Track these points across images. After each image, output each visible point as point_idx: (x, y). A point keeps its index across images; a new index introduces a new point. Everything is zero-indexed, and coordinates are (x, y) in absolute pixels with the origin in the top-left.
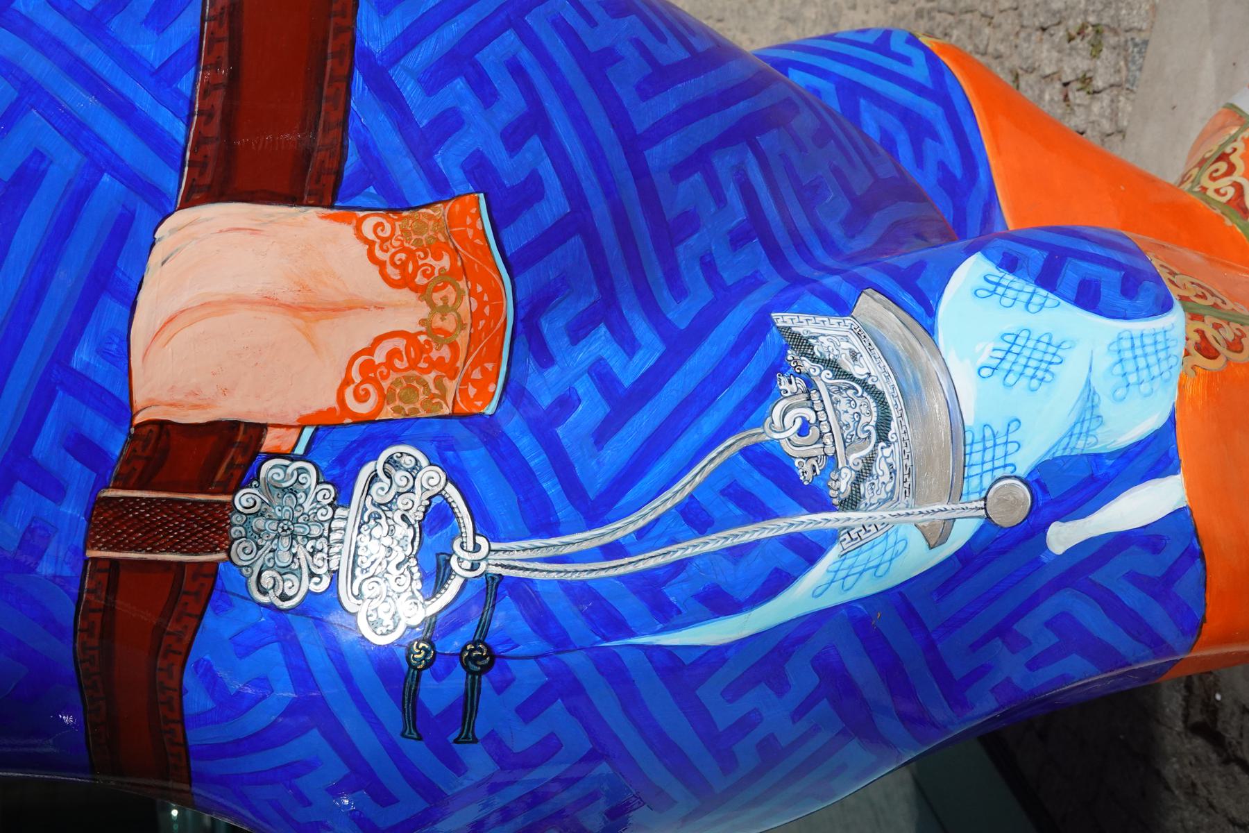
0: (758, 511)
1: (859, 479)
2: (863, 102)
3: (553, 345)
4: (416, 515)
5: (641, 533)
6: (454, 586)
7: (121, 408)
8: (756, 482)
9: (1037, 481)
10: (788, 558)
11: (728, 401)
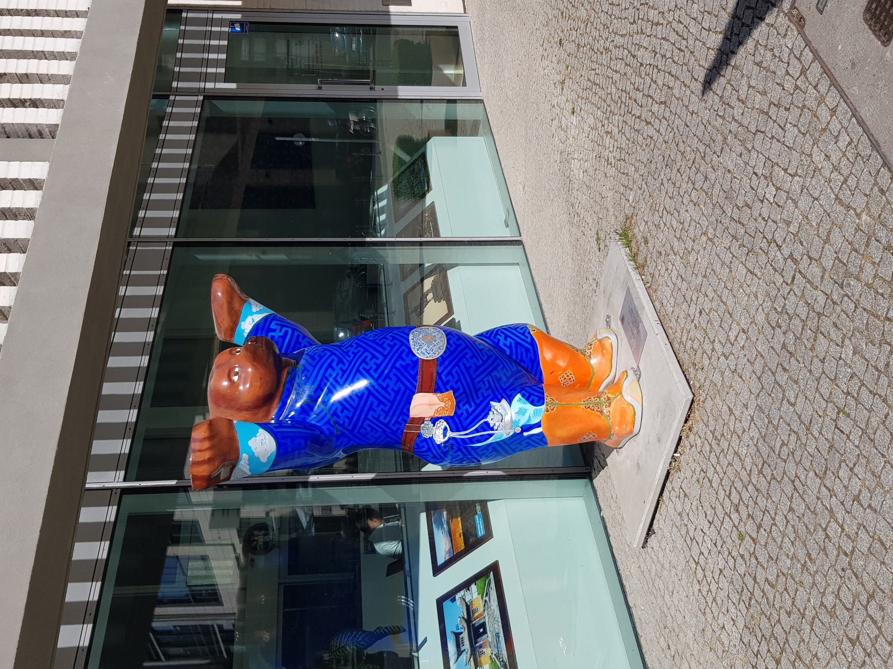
0: (485, 430)
8: (486, 427)
9: (522, 428)
10: (488, 436)
11: (483, 415)
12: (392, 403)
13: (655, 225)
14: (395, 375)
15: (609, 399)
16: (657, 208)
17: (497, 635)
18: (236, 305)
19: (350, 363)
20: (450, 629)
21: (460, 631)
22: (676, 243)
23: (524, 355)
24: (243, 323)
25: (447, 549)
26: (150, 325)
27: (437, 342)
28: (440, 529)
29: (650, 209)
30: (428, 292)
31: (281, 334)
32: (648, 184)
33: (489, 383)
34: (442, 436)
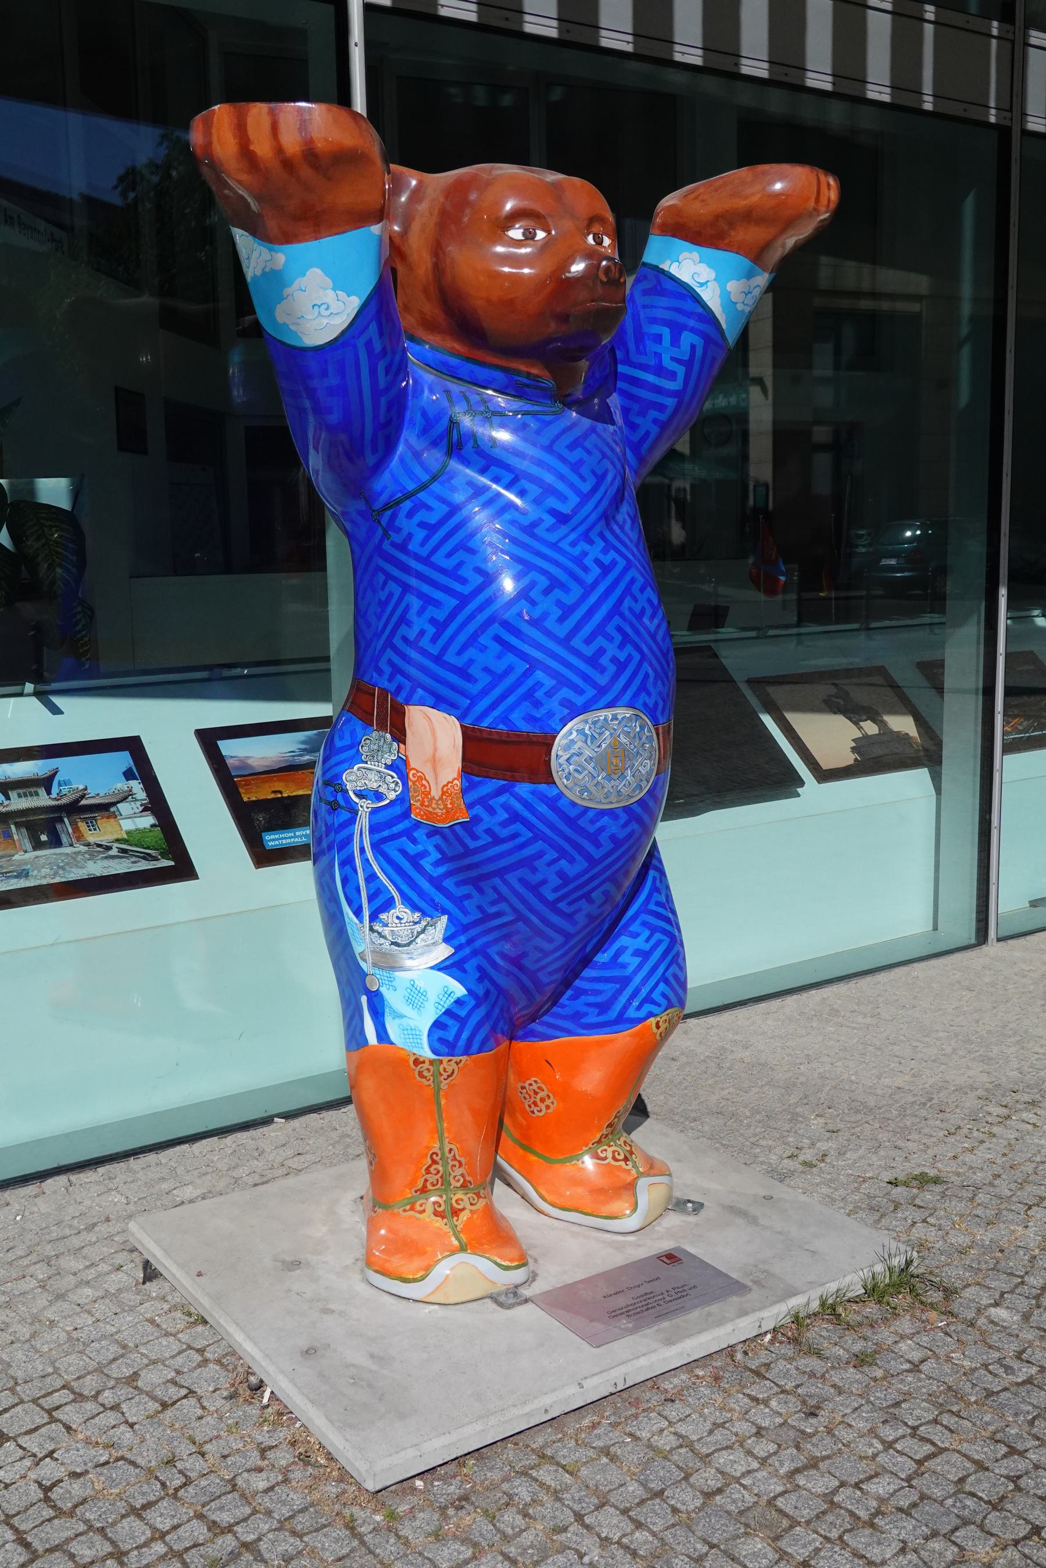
0: (371, 899)
1: (379, 933)
2: (618, 986)
3: (433, 839)
4: (381, 790)
5: (367, 860)
6: (356, 800)
7: (408, 702)
12: (438, 659)
13: (897, 1404)
14: (509, 670)
15: (456, 1213)
16: (946, 1419)
17: (24, 874)
18: (753, 234)
19: (554, 546)
20: (65, 765)
21: (55, 790)
22: (818, 1483)
23: (592, 999)
24: (695, 255)
25: (250, 762)
26: (786, 70)
27: (606, 783)
28: (303, 746)
29: (950, 1388)
30: (882, 724)
31: (667, 363)
32: (1023, 1391)
33: (499, 915)
34: (360, 786)
